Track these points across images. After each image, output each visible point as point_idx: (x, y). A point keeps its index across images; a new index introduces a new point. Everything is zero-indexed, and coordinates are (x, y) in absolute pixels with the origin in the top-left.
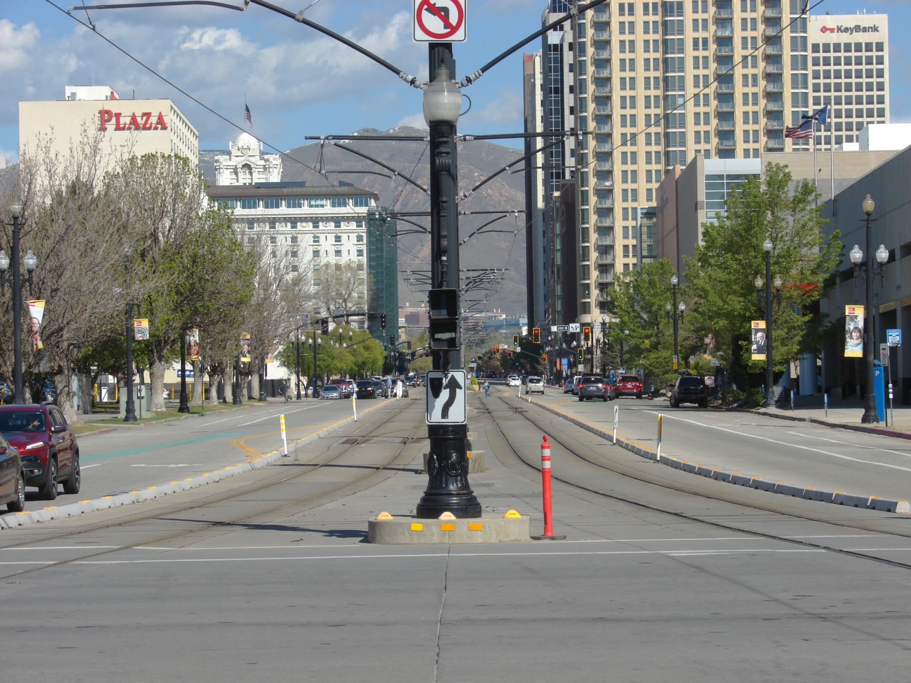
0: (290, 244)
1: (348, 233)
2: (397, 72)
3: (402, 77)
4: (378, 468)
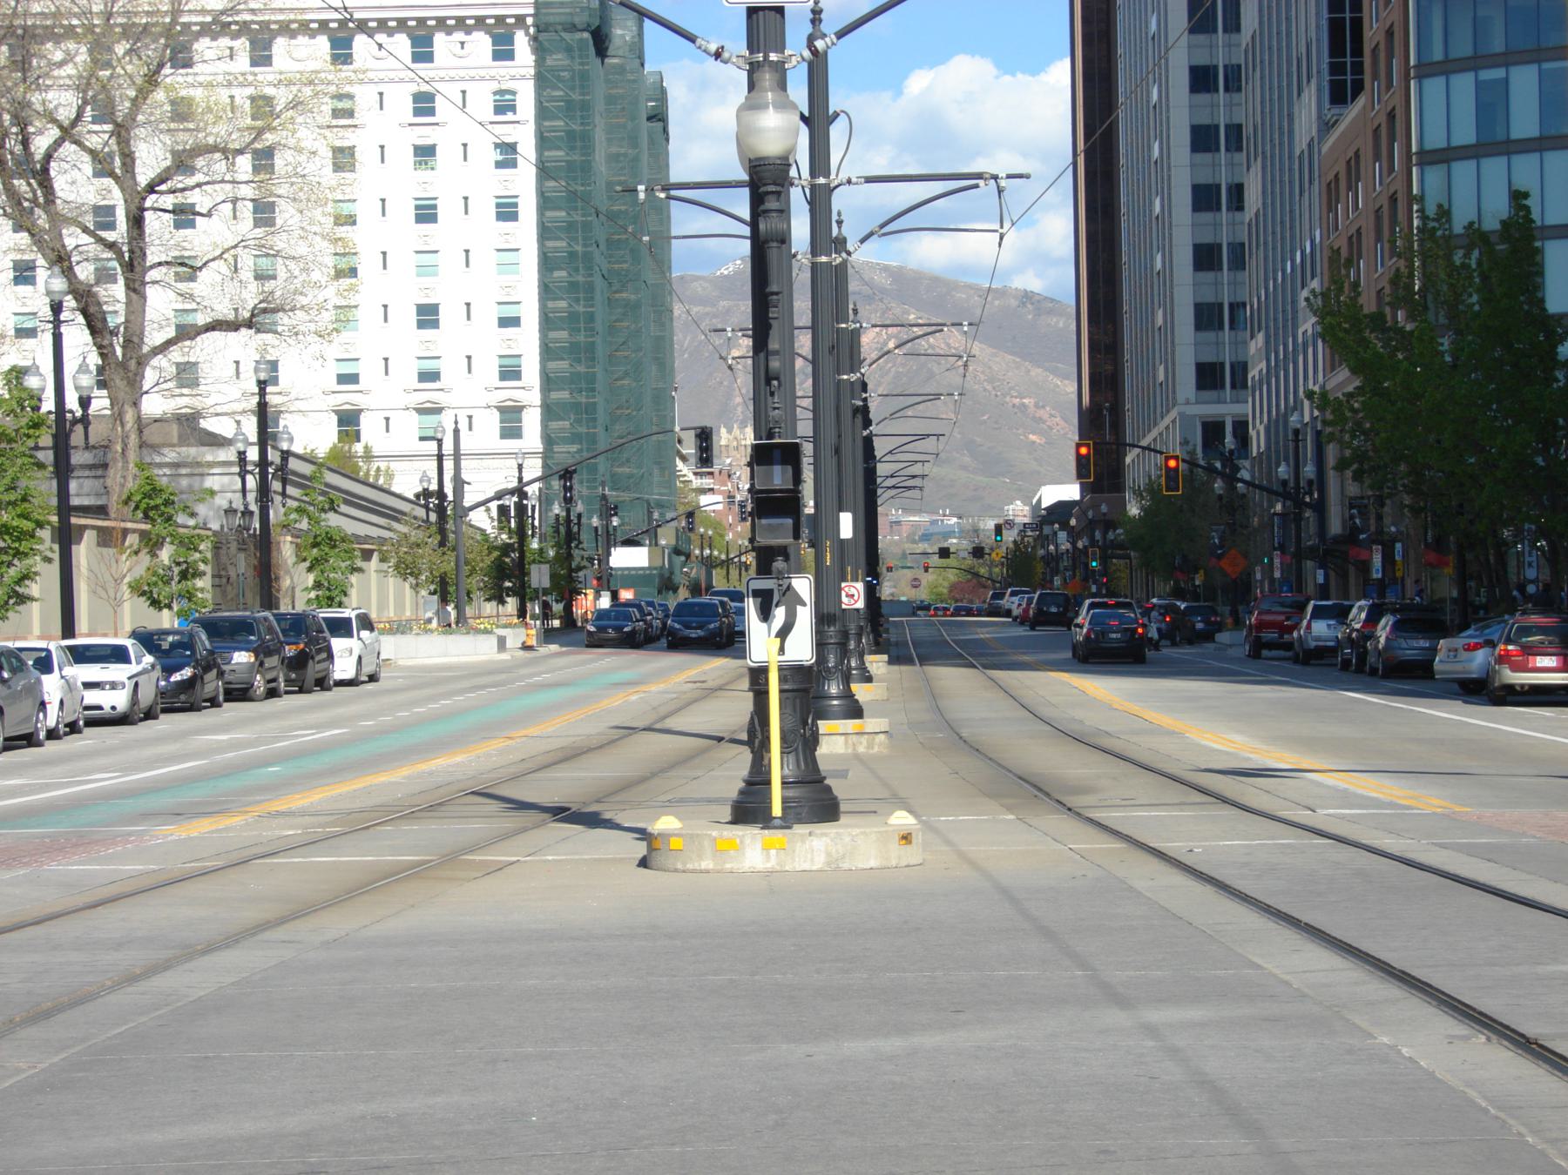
0: (249, 121)
1: (462, 79)
2: (691, 39)
3: (699, 48)
4: (720, 739)
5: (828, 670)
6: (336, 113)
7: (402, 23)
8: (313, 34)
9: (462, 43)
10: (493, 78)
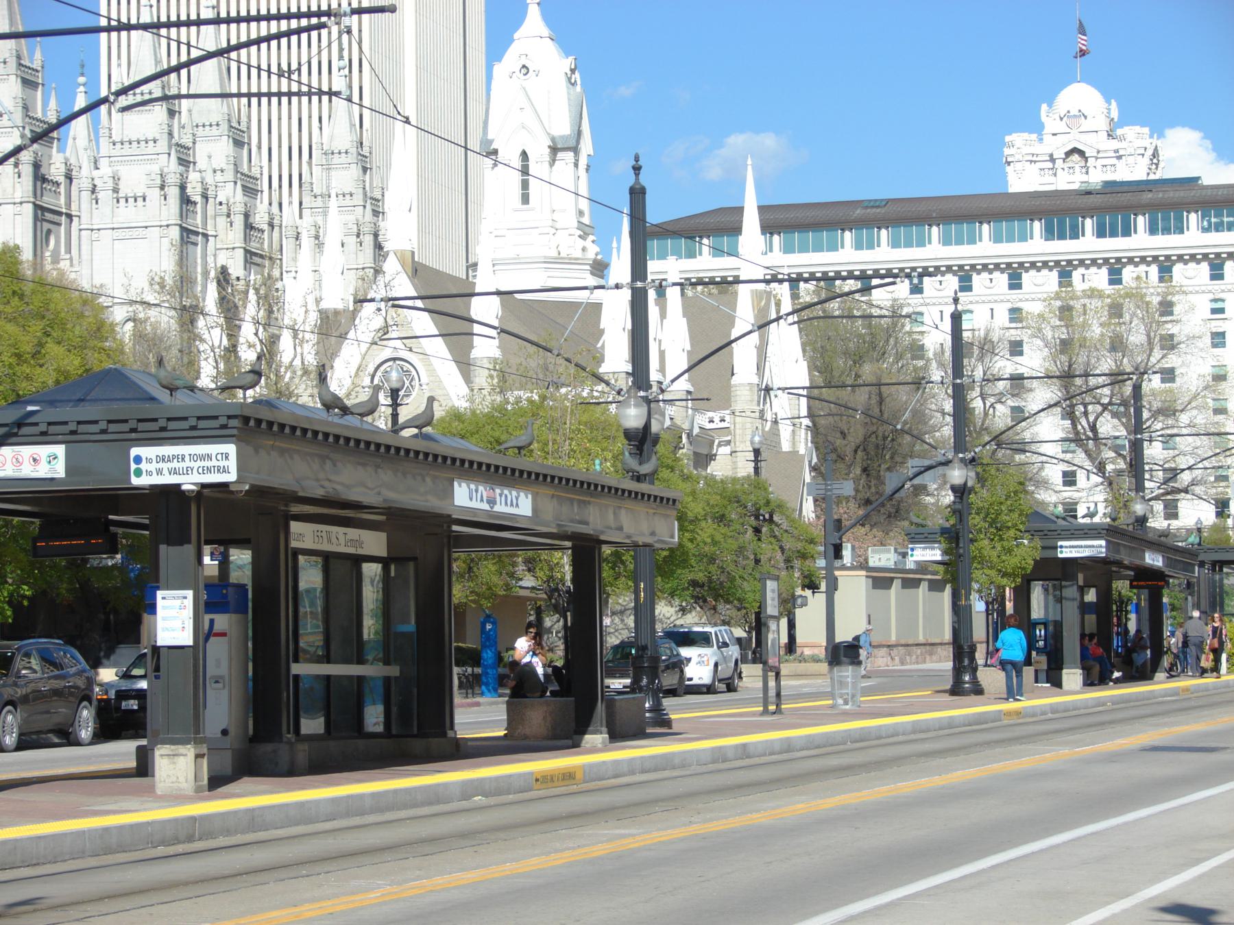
1: (940, 304)
5: (964, 667)
6: (1214, 311)
7: (1205, 257)
8: (1198, 262)
9: (941, 282)
10: (1210, 292)
